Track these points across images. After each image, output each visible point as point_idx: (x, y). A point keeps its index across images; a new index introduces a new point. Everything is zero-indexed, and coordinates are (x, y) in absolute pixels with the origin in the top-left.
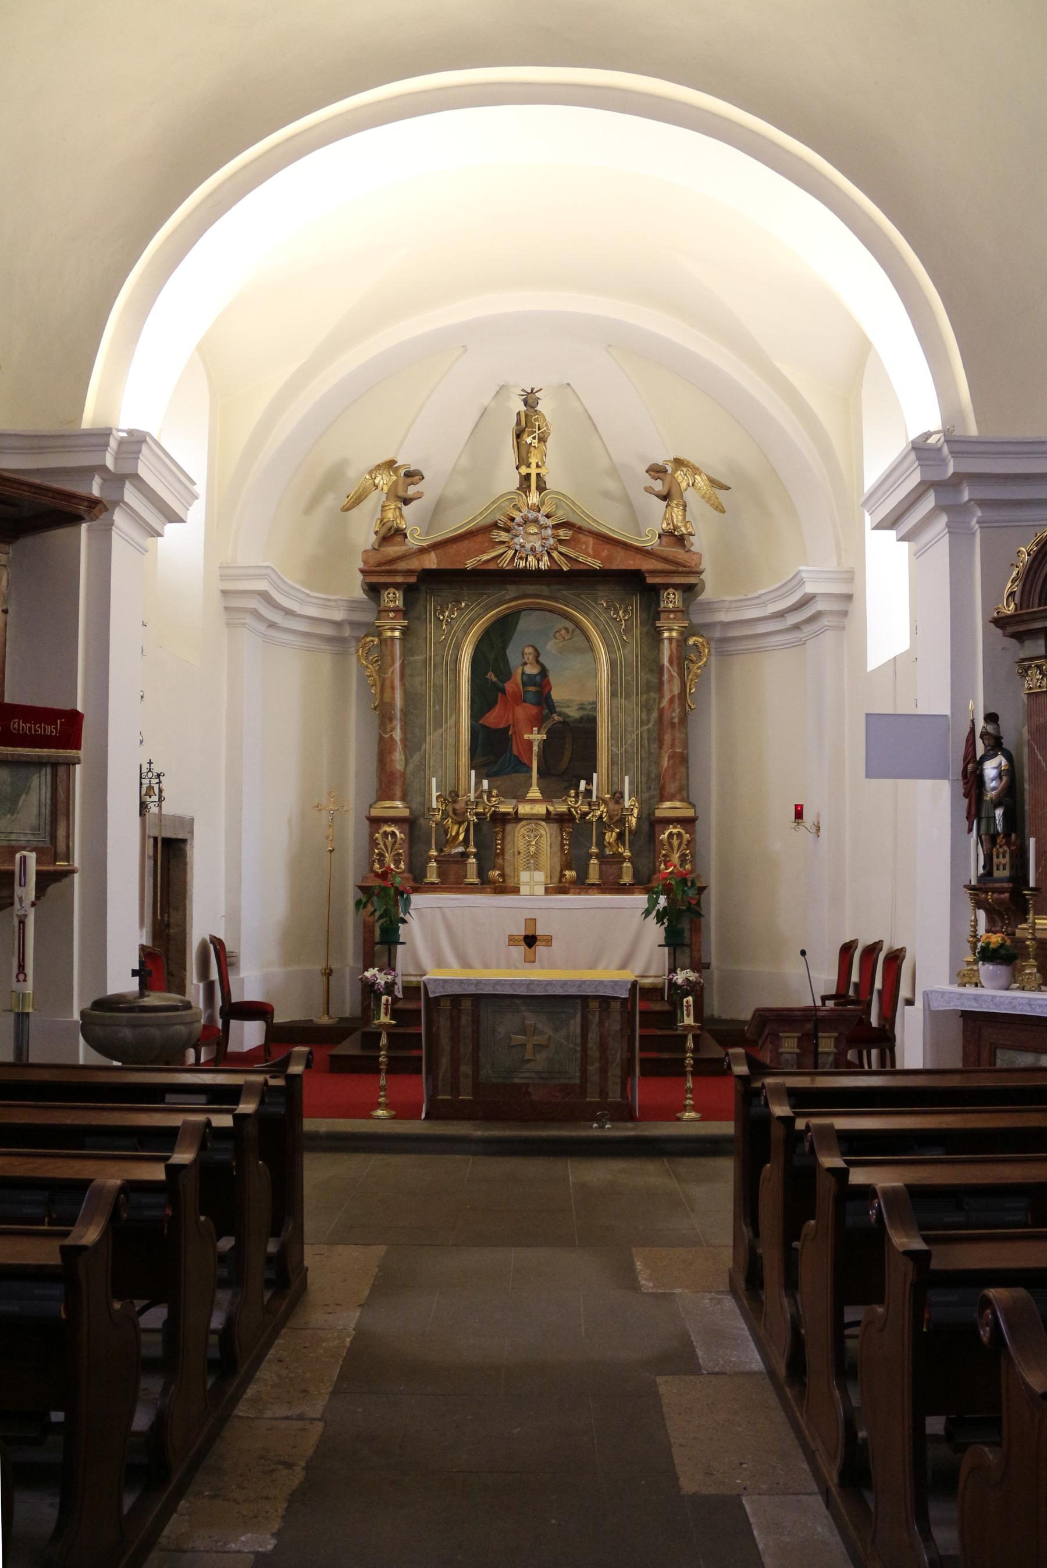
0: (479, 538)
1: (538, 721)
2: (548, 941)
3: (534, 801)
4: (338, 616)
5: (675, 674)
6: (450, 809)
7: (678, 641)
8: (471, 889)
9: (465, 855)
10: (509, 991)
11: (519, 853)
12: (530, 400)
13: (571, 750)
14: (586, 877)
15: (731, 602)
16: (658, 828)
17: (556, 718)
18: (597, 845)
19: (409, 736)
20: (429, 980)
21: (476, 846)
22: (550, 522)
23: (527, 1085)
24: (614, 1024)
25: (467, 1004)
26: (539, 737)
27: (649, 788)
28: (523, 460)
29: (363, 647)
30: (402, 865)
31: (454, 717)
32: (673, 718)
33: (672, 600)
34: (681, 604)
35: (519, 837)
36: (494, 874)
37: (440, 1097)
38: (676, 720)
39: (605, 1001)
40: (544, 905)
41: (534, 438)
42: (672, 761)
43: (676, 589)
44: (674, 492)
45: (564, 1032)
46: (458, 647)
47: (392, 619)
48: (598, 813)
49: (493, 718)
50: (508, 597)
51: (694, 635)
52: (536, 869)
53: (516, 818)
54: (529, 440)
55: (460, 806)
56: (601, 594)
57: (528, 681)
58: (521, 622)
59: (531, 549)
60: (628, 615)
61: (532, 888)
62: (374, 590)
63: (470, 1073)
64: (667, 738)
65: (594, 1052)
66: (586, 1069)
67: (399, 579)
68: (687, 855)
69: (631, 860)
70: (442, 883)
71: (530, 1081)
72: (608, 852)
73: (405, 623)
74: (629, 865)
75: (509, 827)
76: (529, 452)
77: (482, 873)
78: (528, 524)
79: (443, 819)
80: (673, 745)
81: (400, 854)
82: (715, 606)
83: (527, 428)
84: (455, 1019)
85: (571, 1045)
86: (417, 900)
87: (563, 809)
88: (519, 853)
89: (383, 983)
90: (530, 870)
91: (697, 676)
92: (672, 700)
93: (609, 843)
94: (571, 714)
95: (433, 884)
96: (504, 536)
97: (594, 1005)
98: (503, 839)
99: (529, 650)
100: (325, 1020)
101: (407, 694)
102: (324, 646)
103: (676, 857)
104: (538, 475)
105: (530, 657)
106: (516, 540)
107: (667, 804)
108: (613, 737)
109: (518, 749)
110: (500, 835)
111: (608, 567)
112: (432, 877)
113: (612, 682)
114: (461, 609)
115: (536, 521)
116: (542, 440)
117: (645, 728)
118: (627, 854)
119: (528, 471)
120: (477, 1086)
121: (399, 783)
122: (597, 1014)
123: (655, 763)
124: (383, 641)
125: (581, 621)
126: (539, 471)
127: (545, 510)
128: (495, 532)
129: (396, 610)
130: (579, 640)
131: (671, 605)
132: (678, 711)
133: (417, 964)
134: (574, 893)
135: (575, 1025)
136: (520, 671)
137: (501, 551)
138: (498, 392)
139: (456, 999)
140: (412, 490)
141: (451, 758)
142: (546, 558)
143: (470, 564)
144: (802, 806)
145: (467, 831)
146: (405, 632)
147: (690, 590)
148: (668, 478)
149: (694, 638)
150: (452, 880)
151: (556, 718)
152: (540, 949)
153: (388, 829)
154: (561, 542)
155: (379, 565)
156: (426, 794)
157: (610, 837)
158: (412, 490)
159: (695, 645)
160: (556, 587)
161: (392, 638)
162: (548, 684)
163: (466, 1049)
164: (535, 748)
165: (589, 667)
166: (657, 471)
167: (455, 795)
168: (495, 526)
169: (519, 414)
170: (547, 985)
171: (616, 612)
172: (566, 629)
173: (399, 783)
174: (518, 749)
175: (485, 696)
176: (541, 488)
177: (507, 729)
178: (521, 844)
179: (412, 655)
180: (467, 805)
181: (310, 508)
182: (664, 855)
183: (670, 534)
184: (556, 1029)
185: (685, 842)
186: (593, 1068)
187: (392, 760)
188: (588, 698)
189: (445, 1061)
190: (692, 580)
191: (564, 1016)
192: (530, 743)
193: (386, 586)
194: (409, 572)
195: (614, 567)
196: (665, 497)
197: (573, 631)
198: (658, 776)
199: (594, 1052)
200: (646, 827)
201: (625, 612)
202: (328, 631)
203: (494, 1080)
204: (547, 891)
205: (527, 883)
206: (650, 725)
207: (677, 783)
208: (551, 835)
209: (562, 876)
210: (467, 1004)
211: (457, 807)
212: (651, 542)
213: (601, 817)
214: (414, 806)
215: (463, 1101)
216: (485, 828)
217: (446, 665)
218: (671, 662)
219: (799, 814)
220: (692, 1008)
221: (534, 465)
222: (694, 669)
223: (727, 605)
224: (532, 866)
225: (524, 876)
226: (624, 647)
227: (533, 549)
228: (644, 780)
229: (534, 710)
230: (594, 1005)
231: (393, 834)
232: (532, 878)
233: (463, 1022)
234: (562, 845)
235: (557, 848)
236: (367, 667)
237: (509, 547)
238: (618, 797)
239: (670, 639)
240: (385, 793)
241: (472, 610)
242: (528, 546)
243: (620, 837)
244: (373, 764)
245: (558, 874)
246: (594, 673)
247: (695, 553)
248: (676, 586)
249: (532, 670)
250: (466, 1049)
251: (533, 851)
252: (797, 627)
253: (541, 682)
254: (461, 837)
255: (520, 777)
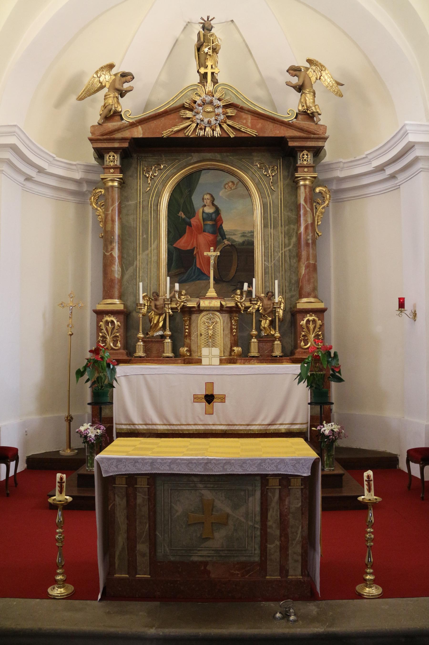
0: (172, 116)
1: (215, 244)
2: (223, 399)
3: (211, 298)
4: (78, 176)
5: (308, 209)
6: (153, 304)
7: (310, 187)
8: (167, 361)
9: (163, 337)
10: (185, 470)
11: (201, 335)
12: (207, 27)
13: (236, 264)
14: (249, 352)
15: (344, 163)
16: (299, 316)
17: (226, 242)
18: (256, 329)
19: (125, 256)
20: (102, 459)
21: (170, 330)
22: (221, 104)
23: (206, 564)
24: (295, 502)
25: (142, 484)
26: (215, 254)
27: (290, 290)
28: (201, 64)
29: (94, 196)
30: (119, 344)
31: (156, 242)
32: (308, 240)
33: (306, 158)
34: (312, 161)
35: (201, 322)
36: (183, 350)
37: (117, 575)
38: (310, 241)
39: (285, 479)
40: (220, 372)
41: (209, 49)
42: (308, 270)
43: (308, 151)
44: (306, 83)
45: (243, 510)
46: (159, 195)
47: (113, 173)
48: (257, 307)
49: (182, 244)
50: (192, 161)
51: (319, 186)
52: (213, 346)
53: (199, 310)
54: (206, 50)
55: (160, 303)
56: (256, 159)
57: (207, 217)
58: (201, 177)
59: (208, 124)
60: (275, 173)
61: (210, 360)
62: (100, 154)
63: (148, 551)
64: (304, 254)
65: (274, 530)
66: (266, 547)
67: (116, 145)
68: (319, 335)
69: (280, 339)
70: (147, 356)
71: (208, 559)
72: (263, 334)
73: (121, 176)
74: (279, 342)
75: (194, 317)
76: (206, 59)
77: (175, 350)
78: (205, 106)
79: (148, 312)
80: (308, 259)
81: (117, 336)
82: (334, 166)
83: (205, 45)
84: (130, 498)
85: (250, 523)
86: (121, 370)
87: (232, 304)
88: (201, 335)
89: (93, 436)
90: (209, 347)
91: (322, 213)
92: (306, 228)
93: (264, 328)
94: (237, 240)
95: (140, 357)
96: (189, 114)
97: (274, 483)
98: (190, 325)
99: (207, 197)
100: (68, 453)
101: (122, 227)
102: (70, 198)
103: (312, 336)
104: (213, 73)
105: (208, 202)
106: (197, 117)
107: (305, 300)
108: (266, 255)
109: (200, 263)
110: (187, 323)
111: (261, 135)
112: (140, 353)
113: (265, 218)
114: (160, 169)
115: (211, 103)
116: (215, 50)
117: (288, 248)
118: (277, 335)
119: (206, 71)
120: (154, 564)
121: (117, 287)
122: (277, 492)
123: (294, 272)
124: (107, 189)
125: (242, 177)
126: (213, 71)
127: (217, 95)
128: (183, 111)
129: (114, 168)
130: (241, 189)
131: (305, 163)
132: (311, 235)
133: (127, 417)
134: (240, 363)
135: (254, 503)
136: (201, 211)
137: (187, 124)
138: (185, 28)
139: (131, 479)
140: (126, 86)
141: (154, 270)
142: (218, 129)
143: (165, 134)
144: (403, 299)
145: (165, 320)
146: (122, 183)
147: (317, 152)
148: (302, 74)
149: (321, 188)
150: (153, 356)
151: (226, 242)
152: (217, 405)
153: (109, 319)
154: (229, 117)
155: (102, 135)
156: (136, 295)
157: (265, 323)
158: (126, 86)
159: (320, 192)
160: (225, 154)
161: (112, 187)
162: (221, 219)
163: (142, 528)
164: (212, 262)
165: (249, 207)
166: (294, 70)
167: (156, 295)
168: (183, 107)
169: (199, 33)
170: (225, 464)
171: (267, 171)
172: (232, 182)
173: (117, 287)
174: (200, 263)
175: (176, 229)
176: (215, 81)
177: (193, 250)
178: (202, 328)
179: (128, 201)
180: (164, 301)
181: (60, 103)
182: (303, 336)
183: (305, 113)
184: (235, 507)
185: (318, 326)
186: (273, 547)
187: (112, 271)
188: (247, 229)
189: (121, 540)
190: (320, 144)
191: (242, 493)
192: (208, 258)
193: (108, 150)
194: (123, 140)
195: (266, 135)
196: (300, 89)
197: (237, 185)
198: (298, 282)
199: (274, 530)
200: (289, 316)
201: (273, 170)
202: (72, 187)
203: (172, 559)
204: (222, 362)
205: (207, 357)
206: (291, 247)
207: (311, 286)
208: (224, 322)
209: (232, 351)
210: (142, 484)
211: (158, 303)
212: (291, 118)
213: (258, 310)
214: (129, 303)
215: (140, 580)
216: (178, 318)
217: (151, 207)
218: (305, 201)
219: (402, 304)
220: (372, 483)
221: (209, 67)
222: (320, 208)
223: (341, 165)
224: (211, 344)
225: (205, 351)
226: (272, 194)
227: (209, 122)
228: (287, 284)
229: (211, 237)
230: (274, 483)
231: (112, 322)
232: (210, 353)
233: (139, 501)
234: (231, 329)
235: (228, 331)
236: (97, 209)
237: (193, 122)
238: (270, 295)
239: (305, 186)
240: (107, 294)
241: (168, 170)
242: (206, 120)
243: (272, 323)
244: (101, 274)
245: (228, 350)
246: (252, 211)
247: (321, 125)
248: (308, 149)
249: (209, 210)
250: (142, 528)
251: (211, 332)
252: (393, 177)
253: (215, 219)
254: (161, 324)
255: (202, 283)
